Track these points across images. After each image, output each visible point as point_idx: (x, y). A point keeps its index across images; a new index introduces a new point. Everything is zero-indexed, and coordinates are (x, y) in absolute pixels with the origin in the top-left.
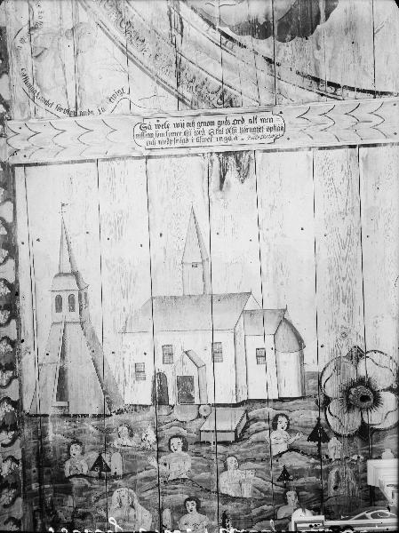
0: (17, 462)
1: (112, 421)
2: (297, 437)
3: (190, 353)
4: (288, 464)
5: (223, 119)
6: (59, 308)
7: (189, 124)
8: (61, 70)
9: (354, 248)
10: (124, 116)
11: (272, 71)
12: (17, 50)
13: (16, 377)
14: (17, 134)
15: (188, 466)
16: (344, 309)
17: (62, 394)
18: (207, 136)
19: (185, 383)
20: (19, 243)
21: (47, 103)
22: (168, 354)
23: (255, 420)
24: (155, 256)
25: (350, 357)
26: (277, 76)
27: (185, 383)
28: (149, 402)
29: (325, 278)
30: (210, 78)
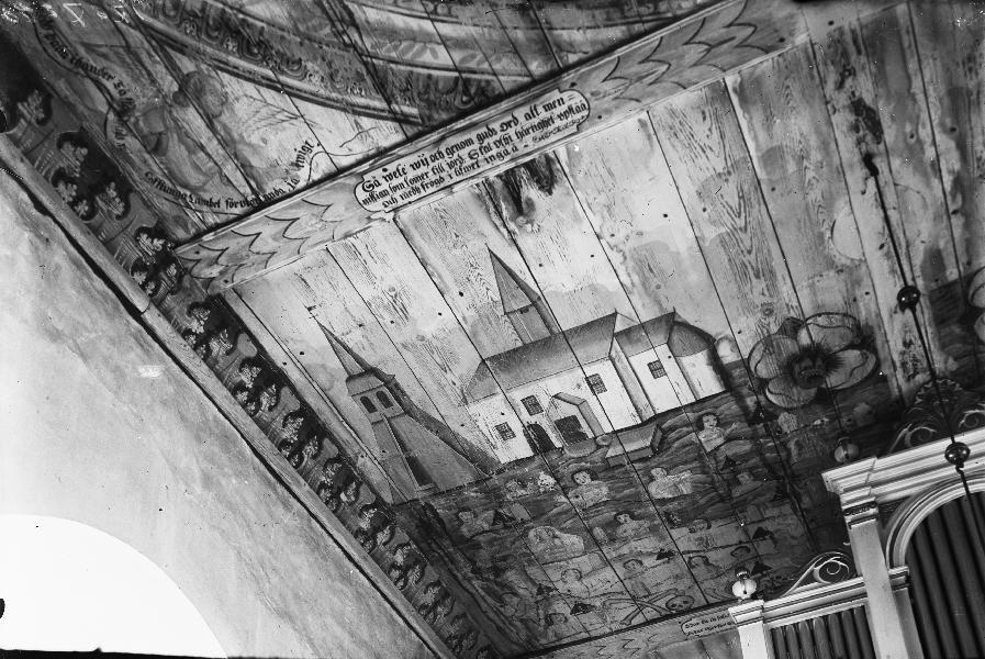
0: (408, 544)
1: (496, 480)
2: (734, 426)
3: (560, 395)
4: (729, 453)
5: (483, 130)
6: (370, 408)
7: (434, 158)
8: (201, 154)
9: (755, 211)
10: (338, 219)
11: (532, 21)
12: (122, 150)
13: (361, 483)
14: (198, 261)
15: (605, 490)
16: (759, 285)
17: (422, 476)
18: (468, 162)
19: (569, 427)
20: (280, 365)
21: (210, 203)
22: (532, 405)
23: (672, 429)
24: (464, 318)
25: (782, 330)
26: (544, 26)
27: (569, 427)
28: (530, 453)
29: (720, 259)
30: (435, 73)
